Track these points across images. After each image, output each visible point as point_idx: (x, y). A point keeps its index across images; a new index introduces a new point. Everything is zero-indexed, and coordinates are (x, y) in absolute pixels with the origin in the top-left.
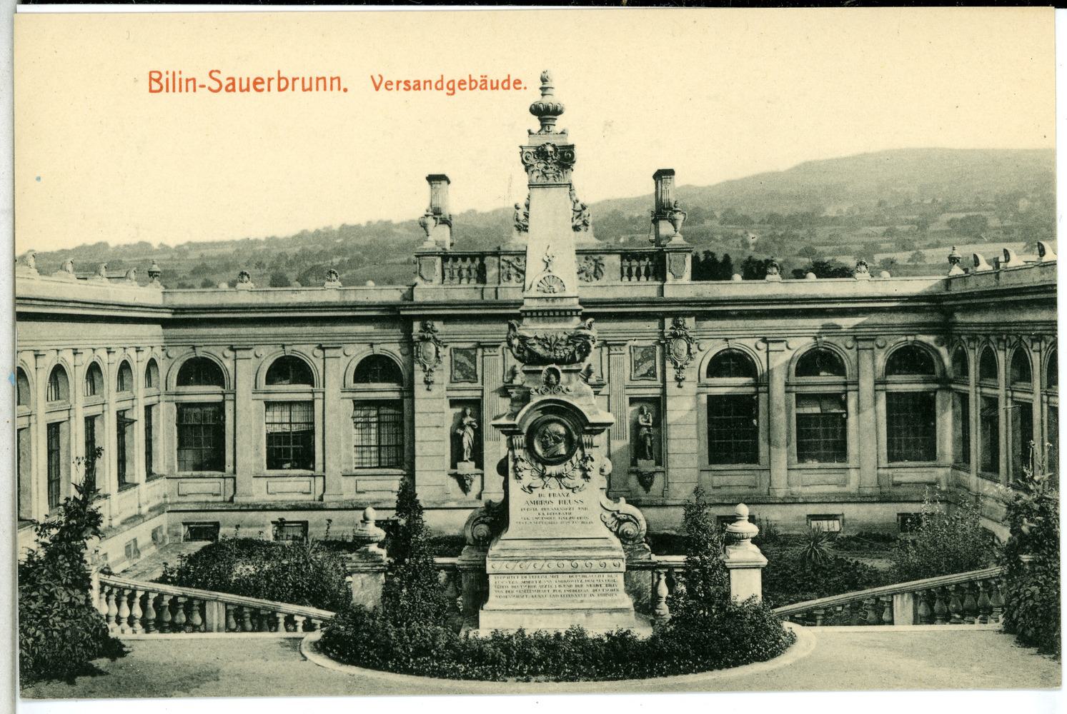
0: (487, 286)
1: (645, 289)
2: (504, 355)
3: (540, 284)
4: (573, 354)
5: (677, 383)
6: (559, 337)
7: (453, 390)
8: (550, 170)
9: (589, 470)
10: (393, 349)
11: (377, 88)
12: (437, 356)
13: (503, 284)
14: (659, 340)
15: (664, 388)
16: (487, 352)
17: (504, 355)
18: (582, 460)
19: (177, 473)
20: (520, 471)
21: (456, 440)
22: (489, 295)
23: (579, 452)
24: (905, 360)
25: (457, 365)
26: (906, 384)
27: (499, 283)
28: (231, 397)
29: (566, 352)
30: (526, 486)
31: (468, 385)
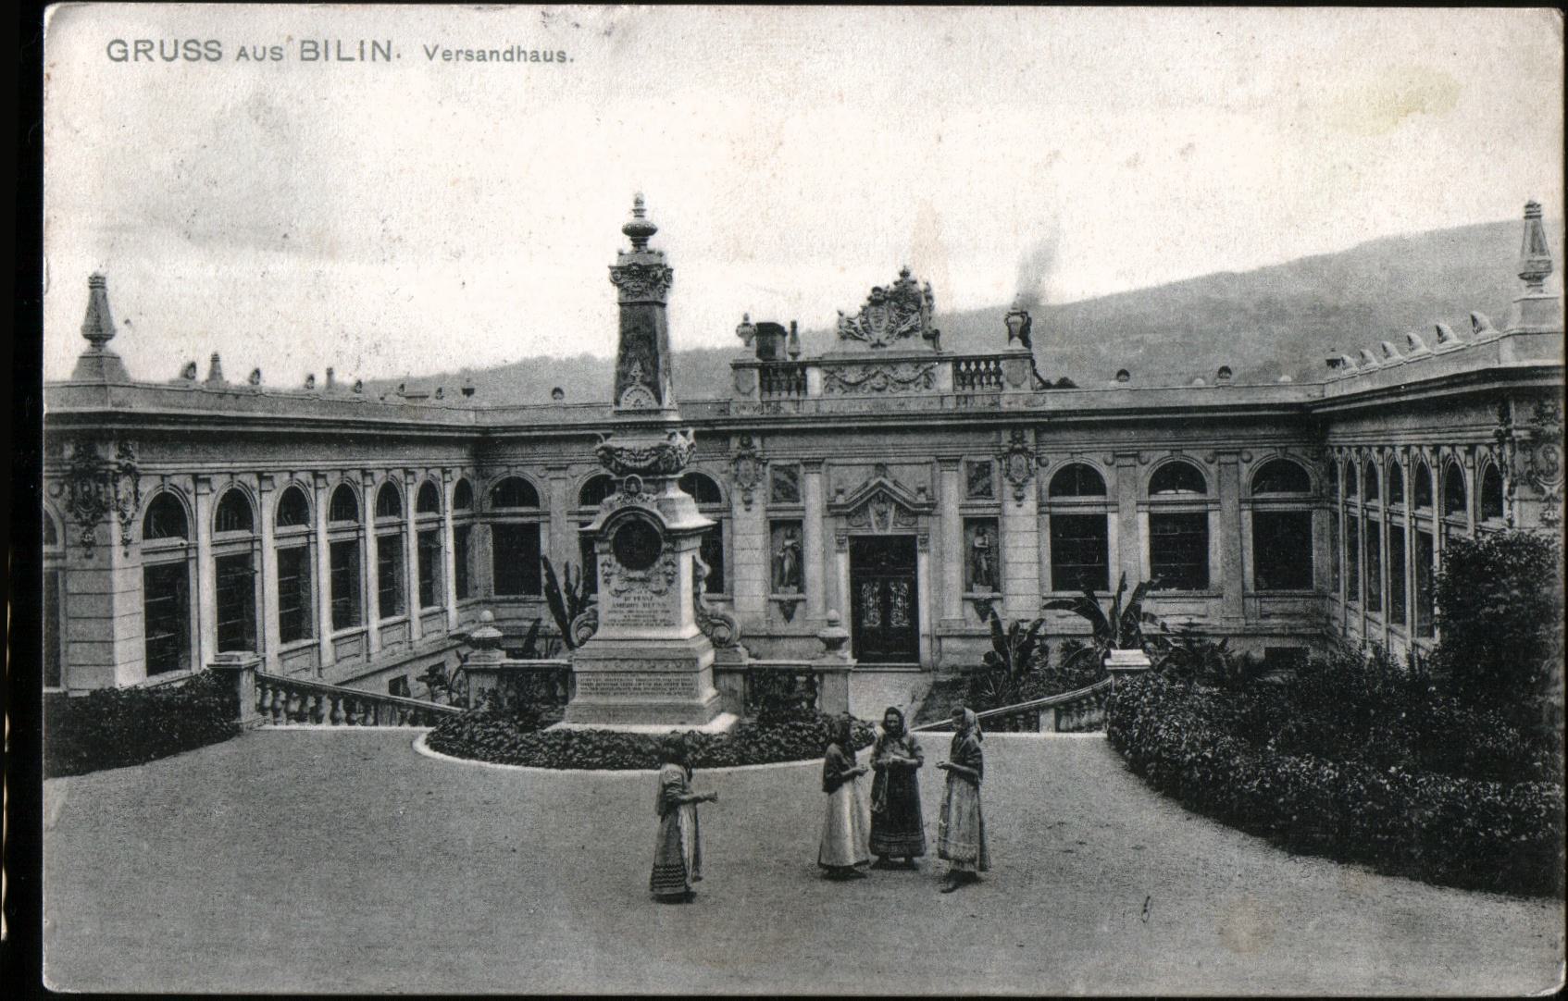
5: (1017, 503)
7: (972, 507)
11: (431, 57)
19: (494, 597)
24: (1268, 476)
25: (778, 484)
26: (1279, 502)
31: (790, 505)
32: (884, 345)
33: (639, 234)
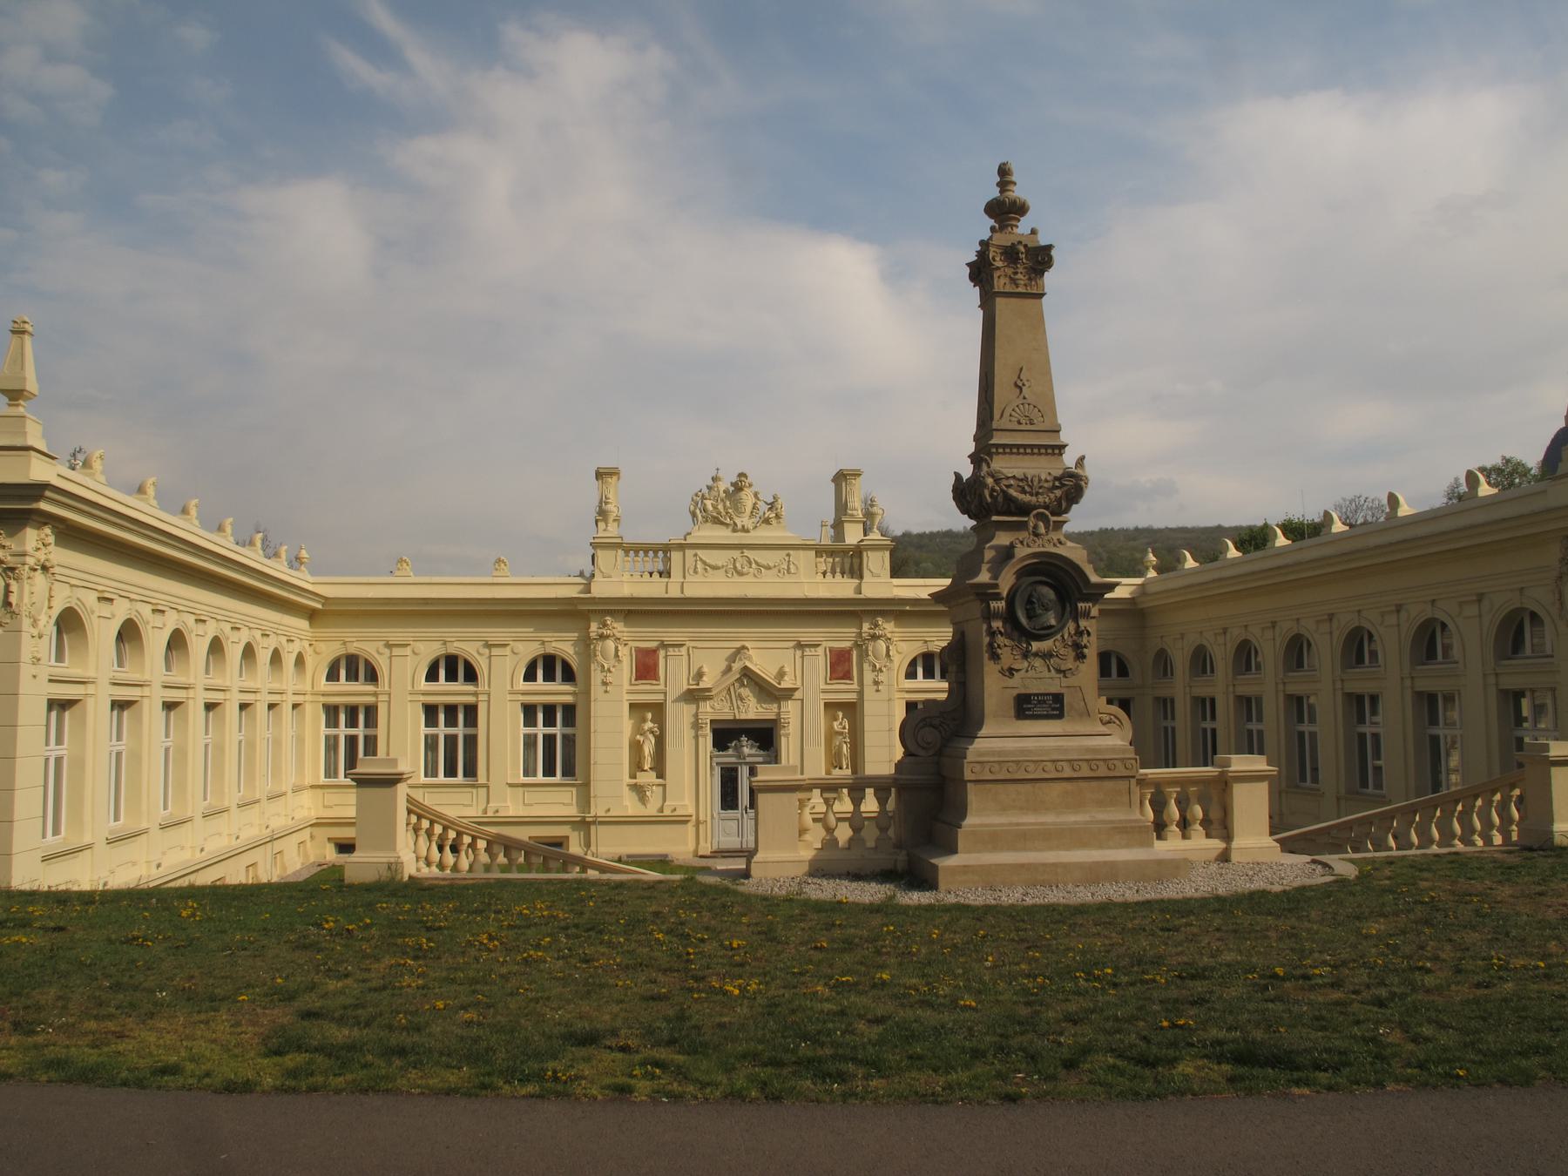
0: (671, 580)
1: (842, 588)
2: (689, 655)
3: (1013, 413)
4: (1059, 500)
6: (1043, 478)
8: (1019, 276)
9: (1086, 647)
10: (564, 645)
12: (617, 655)
13: (689, 578)
14: (856, 641)
15: (861, 693)
16: (671, 651)
17: (689, 655)
18: (1075, 634)
20: (999, 646)
21: (636, 748)
22: (674, 592)
23: (1071, 626)
27: (684, 577)
28: (385, 698)
29: (1052, 496)
30: (1006, 667)
32: (747, 531)
33: (1004, 211)
